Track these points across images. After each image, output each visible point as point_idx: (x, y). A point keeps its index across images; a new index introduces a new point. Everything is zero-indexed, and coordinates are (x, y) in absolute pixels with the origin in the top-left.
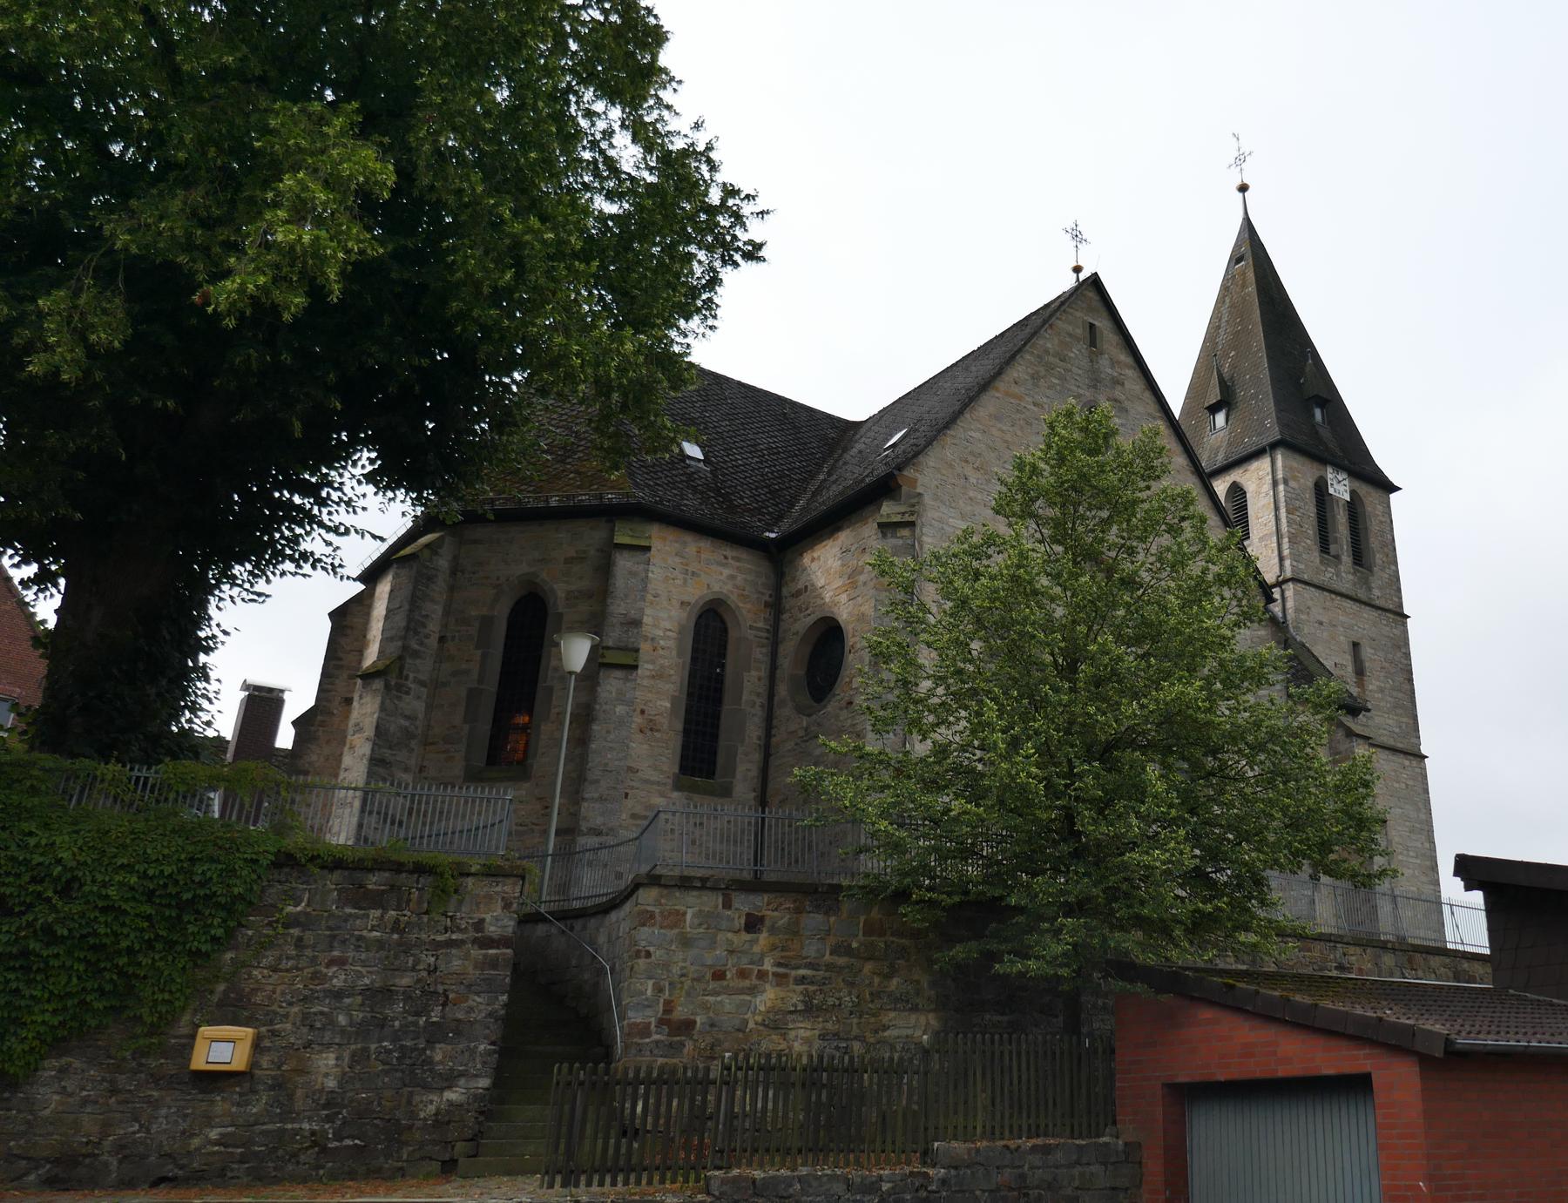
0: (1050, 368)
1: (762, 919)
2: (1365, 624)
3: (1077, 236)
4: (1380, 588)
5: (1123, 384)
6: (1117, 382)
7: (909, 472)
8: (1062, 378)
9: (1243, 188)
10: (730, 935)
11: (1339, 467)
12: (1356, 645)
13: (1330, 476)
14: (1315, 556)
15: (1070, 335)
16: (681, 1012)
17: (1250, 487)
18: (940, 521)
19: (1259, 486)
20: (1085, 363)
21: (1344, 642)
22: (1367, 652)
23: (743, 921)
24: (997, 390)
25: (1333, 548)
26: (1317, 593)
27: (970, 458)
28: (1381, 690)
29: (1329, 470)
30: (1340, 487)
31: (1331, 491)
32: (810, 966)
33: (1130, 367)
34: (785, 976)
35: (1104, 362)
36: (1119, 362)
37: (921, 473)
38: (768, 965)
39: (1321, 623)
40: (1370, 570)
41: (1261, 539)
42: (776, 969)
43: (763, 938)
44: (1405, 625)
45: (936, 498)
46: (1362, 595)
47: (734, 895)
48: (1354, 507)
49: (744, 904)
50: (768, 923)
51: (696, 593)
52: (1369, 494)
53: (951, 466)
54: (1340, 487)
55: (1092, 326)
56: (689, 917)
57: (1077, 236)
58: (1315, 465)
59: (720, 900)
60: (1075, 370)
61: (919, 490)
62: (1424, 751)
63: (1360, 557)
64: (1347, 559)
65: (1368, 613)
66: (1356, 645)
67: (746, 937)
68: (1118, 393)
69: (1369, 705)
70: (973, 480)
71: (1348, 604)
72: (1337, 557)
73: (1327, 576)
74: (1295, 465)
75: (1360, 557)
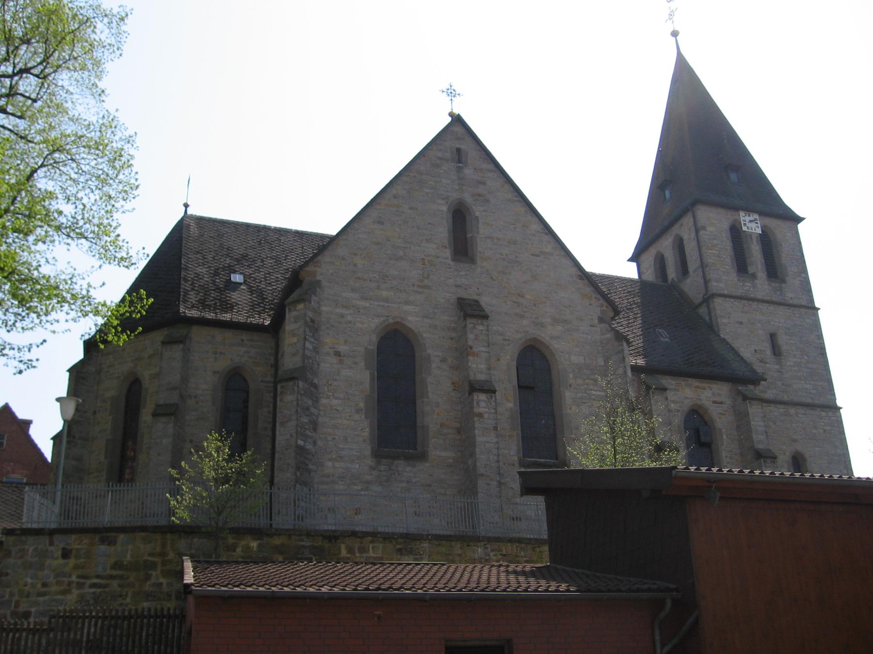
1: (71, 551)
2: (779, 319)
3: (451, 93)
7: (310, 268)
9: (675, 34)
11: (749, 210)
12: (773, 337)
13: (742, 219)
14: (733, 276)
15: (440, 159)
16: (22, 609)
17: (685, 237)
23: (60, 553)
25: (751, 270)
29: (742, 214)
30: (751, 225)
31: (745, 228)
32: (98, 577)
33: (490, 171)
34: (84, 584)
35: (468, 172)
38: (74, 578)
39: (741, 323)
40: (783, 281)
41: (694, 272)
42: (78, 580)
43: (72, 562)
48: (766, 240)
49: (60, 542)
50: (74, 552)
51: (223, 364)
52: (778, 227)
54: (751, 225)
55: (459, 150)
56: (30, 552)
57: (451, 93)
59: (47, 541)
61: (319, 278)
64: (762, 275)
65: (782, 311)
66: (773, 337)
69: (766, 377)
71: (764, 307)
75: (774, 271)
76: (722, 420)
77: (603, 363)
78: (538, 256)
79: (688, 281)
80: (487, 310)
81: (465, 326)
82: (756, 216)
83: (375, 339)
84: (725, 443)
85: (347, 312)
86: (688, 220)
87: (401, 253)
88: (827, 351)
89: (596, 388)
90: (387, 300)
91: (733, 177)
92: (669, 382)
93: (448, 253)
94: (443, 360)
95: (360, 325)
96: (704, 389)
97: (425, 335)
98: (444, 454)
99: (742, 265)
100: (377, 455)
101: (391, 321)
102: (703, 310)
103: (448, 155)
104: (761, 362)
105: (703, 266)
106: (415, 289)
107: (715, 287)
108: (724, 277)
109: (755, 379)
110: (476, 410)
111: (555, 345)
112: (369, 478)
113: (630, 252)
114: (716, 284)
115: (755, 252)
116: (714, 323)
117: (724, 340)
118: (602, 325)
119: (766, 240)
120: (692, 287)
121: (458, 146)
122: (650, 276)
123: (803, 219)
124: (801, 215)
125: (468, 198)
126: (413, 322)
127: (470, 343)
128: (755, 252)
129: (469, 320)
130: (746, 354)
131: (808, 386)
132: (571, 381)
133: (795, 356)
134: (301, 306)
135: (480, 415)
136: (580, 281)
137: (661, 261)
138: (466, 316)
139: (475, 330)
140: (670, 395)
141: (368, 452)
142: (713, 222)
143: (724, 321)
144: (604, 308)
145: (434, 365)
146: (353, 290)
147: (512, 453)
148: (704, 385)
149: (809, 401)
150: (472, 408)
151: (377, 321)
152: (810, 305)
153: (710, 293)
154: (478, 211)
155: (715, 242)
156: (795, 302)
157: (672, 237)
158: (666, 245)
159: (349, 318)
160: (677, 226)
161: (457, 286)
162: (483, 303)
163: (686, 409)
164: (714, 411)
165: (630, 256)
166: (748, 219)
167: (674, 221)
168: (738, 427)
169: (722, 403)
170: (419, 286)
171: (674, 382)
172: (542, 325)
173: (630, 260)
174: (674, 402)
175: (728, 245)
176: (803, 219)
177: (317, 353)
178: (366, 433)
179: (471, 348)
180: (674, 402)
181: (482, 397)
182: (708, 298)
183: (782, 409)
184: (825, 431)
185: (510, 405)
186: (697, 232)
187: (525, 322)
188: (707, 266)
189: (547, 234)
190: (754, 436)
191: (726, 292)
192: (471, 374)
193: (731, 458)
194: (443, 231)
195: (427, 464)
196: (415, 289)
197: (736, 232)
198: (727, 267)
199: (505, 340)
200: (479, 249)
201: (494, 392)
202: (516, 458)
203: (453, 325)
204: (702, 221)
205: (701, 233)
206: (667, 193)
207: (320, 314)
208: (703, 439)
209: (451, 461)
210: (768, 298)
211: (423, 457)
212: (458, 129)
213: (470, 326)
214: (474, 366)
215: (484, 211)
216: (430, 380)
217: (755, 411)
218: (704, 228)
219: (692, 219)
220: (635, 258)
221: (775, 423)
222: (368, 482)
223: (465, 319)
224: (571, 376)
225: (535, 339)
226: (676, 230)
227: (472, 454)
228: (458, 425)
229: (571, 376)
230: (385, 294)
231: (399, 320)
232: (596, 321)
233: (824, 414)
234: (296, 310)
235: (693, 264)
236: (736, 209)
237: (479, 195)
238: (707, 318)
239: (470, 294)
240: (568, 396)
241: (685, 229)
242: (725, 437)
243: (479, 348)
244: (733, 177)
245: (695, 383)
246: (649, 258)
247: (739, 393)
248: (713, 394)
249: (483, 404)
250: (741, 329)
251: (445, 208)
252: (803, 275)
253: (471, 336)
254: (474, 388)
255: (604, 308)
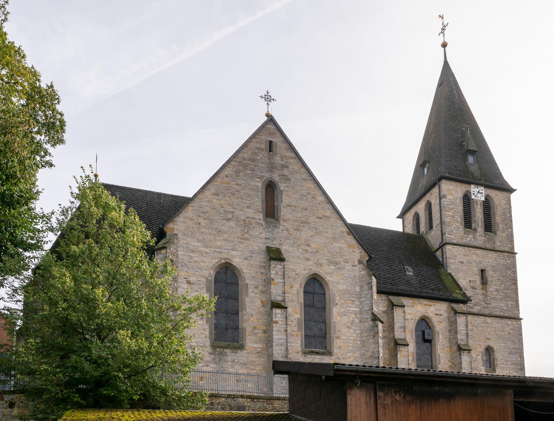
0: (245, 166)
2: (489, 260)
3: (268, 98)
4: (501, 241)
5: (288, 167)
6: (284, 166)
8: (253, 170)
9: (444, 45)
10: (3, 410)
11: (478, 184)
13: (472, 190)
14: (461, 229)
15: (258, 148)
17: (433, 202)
18: (187, 244)
19: (436, 201)
20: (266, 160)
21: (476, 270)
22: (489, 274)
24: (216, 181)
25: (473, 225)
26: (461, 248)
27: (202, 215)
28: (497, 290)
29: (473, 186)
31: (473, 197)
33: (292, 158)
35: (277, 159)
36: (286, 157)
37: (177, 225)
39: (462, 263)
41: (436, 227)
44: (514, 258)
45: (184, 234)
46: (488, 246)
47: (4, 396)
48: (487, 205)
50: (17, 404)
53: (192, 219)
54: (478, 194)
55: (271, 142)
57: (268, 98)
58: (464, 185)
60: (260, 165)
61: (176, 232)
62: (521, 316)
63: (489, 227)
64: (480, 229)
66: (483, 271)
67: (9, 410)
68: (285, 172)
70: (203, 224)
71: (479, 252)
72: (475, 230)
73: (469, 239)
74: (451, 187)
75: (489, 227)
76: (440, 326)
77: (359, 290)
78: (321, 218)
79: (433, 233)
80: (285, 255)
81: (270, 266)
82: (482, 188)
83: (213, 273)
84: (440, 340)
85: (194, 255)
86: (435, 190)
87: (230, 216)
88: (518, 282)
89: (353, 306)
90: (220, 247)
91: (471, 159)
92: (406, 301)
93: (261, 216)
94: (256, 287)
95: (203, 264)
96: (430, 306)
97: (245, 271)
98: (255, 345)
99: (468, 222)
100: (214, 347)
101: (223, 261)
102: (438, 254)
103: (263, 146)
104: (473, 288)
105: (442, 223)
106: (240, 240)
107: (448, 237)
108: (455, 230)
109: (465, 300)
110: (274, 319)
111: (328, 278)
112: (209, 359)
113: (398, 213)
114: (448, 236)
115: (478, 213)
116: (445, 262)
117: (450, 274)
118: (361, 265)
119: (487, 205)
120: (433, 238)
121: (271, 139)
122: (410, 230)
123: (515, 190)
124: (514, 188)
125: (276, 178)
126: (237, 262)
127: (272, 276)
128: (478, 213)
129: (272, 262)
130: (463, 282)
131: (502, 305)
132: (337, 302)
133: (496, 285)
134: (163, 251)
135: (277, 322)
136: (348, 236)
137: (417, 217)
138: (271, 259)
139: (276, 268)
140: (406, 309)
141: (208, 344)
142: (452, 192)
143: (452, 261)
144: (363, 254)
145: (250, 290)
146: (198, 241)
147: (298, 345)
148: (430, 303)
149: (502, 314)
150: (272, 318)
151: (214, 261)
152: (511, 251)
153: (444, 242)
154: (282, 186)
155: (452, 206)
156: (502, 248)
157: (425, 202)
158: (421, 207)
159: (196, 259)
160: (428, 195)
161: (266, 239)
162: (283, 252)
163: (417, 318)
164: (435, 320)
165: (399, 214)
166: (476, 190)
167: (429, 189)
168: (450, 331)
169: (441, 315)
170: (241, 238)
171: (411, 301)
172: (321, 265)
173: (399, 217)
174: (410, 314)
175: (460, 208)
176: (515, 190)
177: (176, 282)
178: (207, 333)
179: (273, 280)
180: (410, 314)
181: (278, 311)
182: (442, 246)
183: (482, 319)
184: (509, 333)
185: (299, 316)
186: (440, 199)
187: (310, 263)
188: (444, 223)
189: (328, 203)
190: (459, 336)
191: (455, 242)
192: (272, 296)
193: (443, 349)
194: (258, 201)
195: (245, 352)
196: (240, 240)
197: (467, 199)
198: (458, 224)
199: (296, 274)
200: (282, 213)
201: (286, 308)
202: (300, 349)
203: (263, 264)
204: (444, 191)
205: (443, 200)
206: (426, 170)
207: (177, 256)
208: (427, 337)
209: (260, 350)
210: (483, 246)
211: (241, 347)
212: (271, 126)
213: (273, 265)
214: (275, 291)
215: (287, 187)
216: (247, 299)
217: (461, 320)
218: (445, 196)
219: (438, 190)
220: (402, 216)
221: (477, 327)
222: (208, 362)
223: (270, 261)
224: (338, 298)
225: (316, 274)
226: (427, 197)
227: (272, 346)
228: (265, 328)
229: (338, 298)
230: (219, 243)
231: (228, 261)
232: (357, 263)
233: (510, 323)
234: (160, 254)
235: (436, 222)
236: (469, 183)
237: (283, 175)
238: (441, 259)
239: (274, 244)
240: (335, 310)
241: (433, 197)
242: (440, 336)
243: (278, 280)
244: (471, 159)
245: (425, 302)
246: (410, 216)
247: (453, 309)
248: (436, 310)
249: (279, 316)
250: (462, 265)
251: (260, 185)
252: (510, 230)
253: (273, 272)
254: (276, 305)
255: (363, 254)
